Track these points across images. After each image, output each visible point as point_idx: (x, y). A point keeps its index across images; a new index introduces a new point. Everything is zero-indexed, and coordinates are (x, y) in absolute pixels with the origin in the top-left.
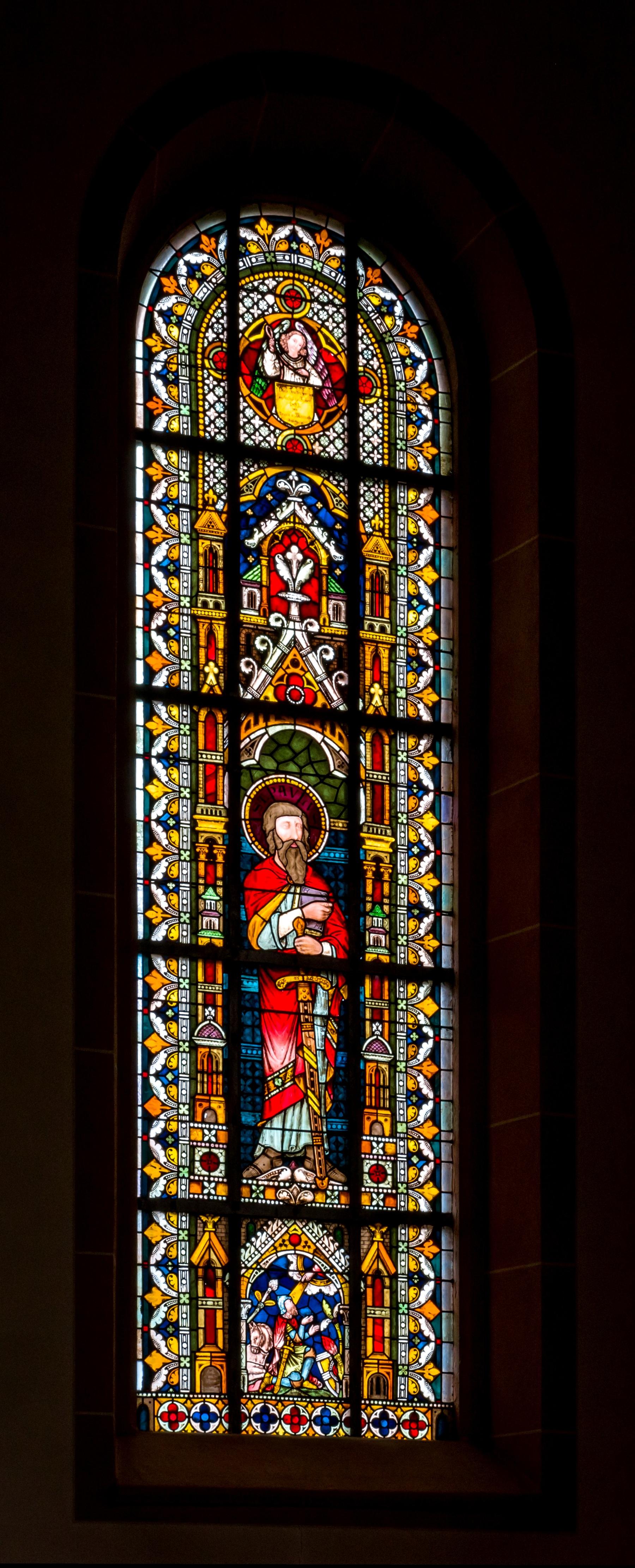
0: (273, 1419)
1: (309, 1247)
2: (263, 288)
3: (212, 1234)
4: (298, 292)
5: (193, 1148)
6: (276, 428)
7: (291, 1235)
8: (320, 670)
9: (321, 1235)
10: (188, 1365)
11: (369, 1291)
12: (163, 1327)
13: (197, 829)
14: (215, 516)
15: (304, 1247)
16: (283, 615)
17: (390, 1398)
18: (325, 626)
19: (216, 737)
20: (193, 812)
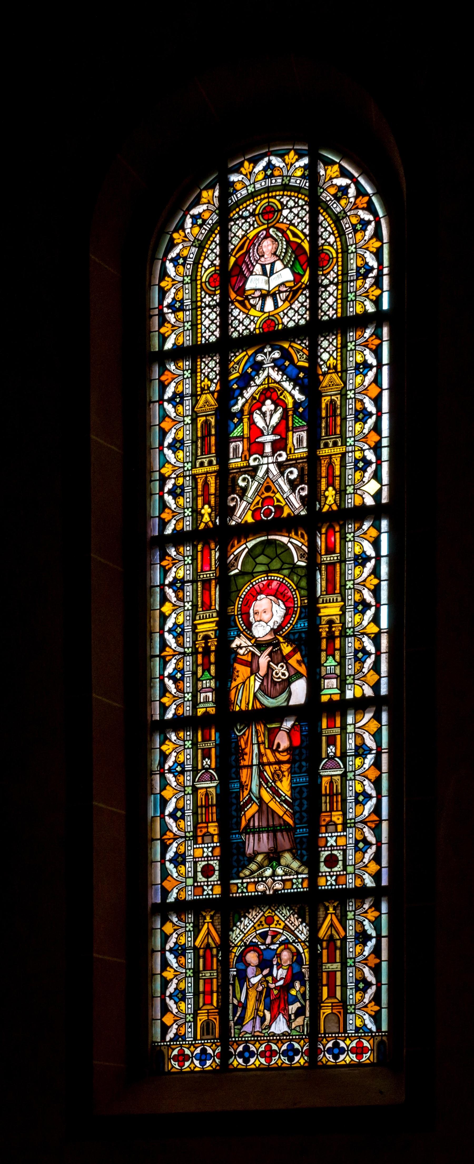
0: (252, 1054)
1: (280, 924)
2: (246, 214)
3: (210, 924)
4: (272, 206)
5: (195, 863)
6: (254, 317)
7: (266, 918)
8: (286, 488)
9: (288, 914)
10: (192, 1020)
11: (325, 952)
12: (175, 858)
13: (197, 631)
14: (209, 397)
15: (276, 925)
16: (259, 455)
17: (342, 1030)
18: (290, 453)
19: (211, 559)
20: (194, 619)
